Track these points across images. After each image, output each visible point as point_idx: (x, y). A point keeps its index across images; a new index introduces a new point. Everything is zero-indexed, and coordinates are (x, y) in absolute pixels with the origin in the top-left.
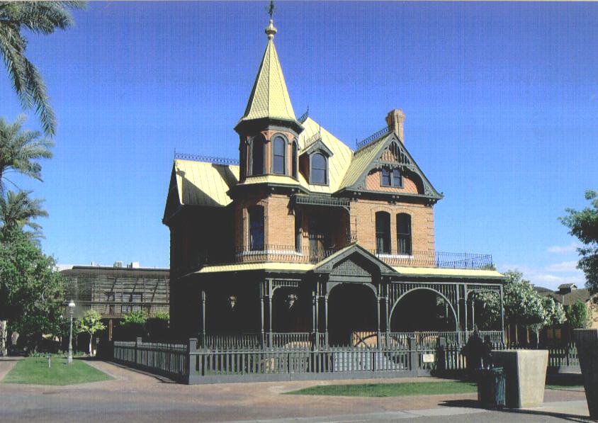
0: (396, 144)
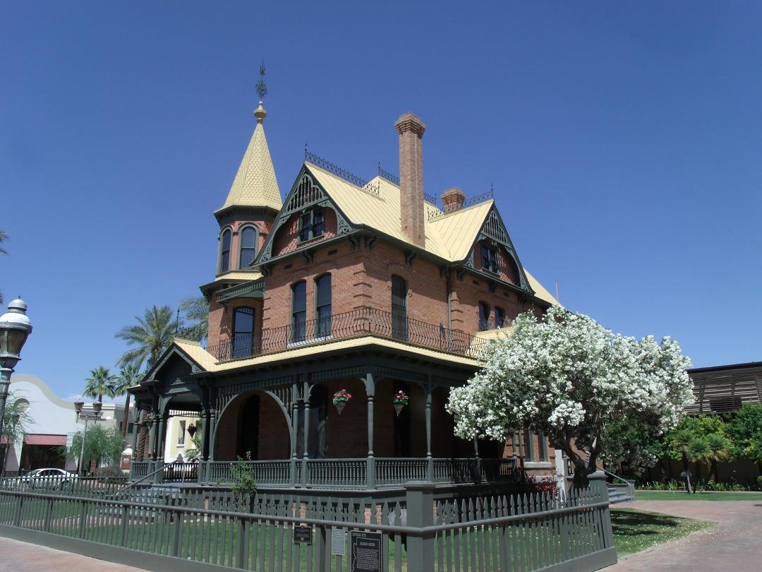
0: (307, 178)
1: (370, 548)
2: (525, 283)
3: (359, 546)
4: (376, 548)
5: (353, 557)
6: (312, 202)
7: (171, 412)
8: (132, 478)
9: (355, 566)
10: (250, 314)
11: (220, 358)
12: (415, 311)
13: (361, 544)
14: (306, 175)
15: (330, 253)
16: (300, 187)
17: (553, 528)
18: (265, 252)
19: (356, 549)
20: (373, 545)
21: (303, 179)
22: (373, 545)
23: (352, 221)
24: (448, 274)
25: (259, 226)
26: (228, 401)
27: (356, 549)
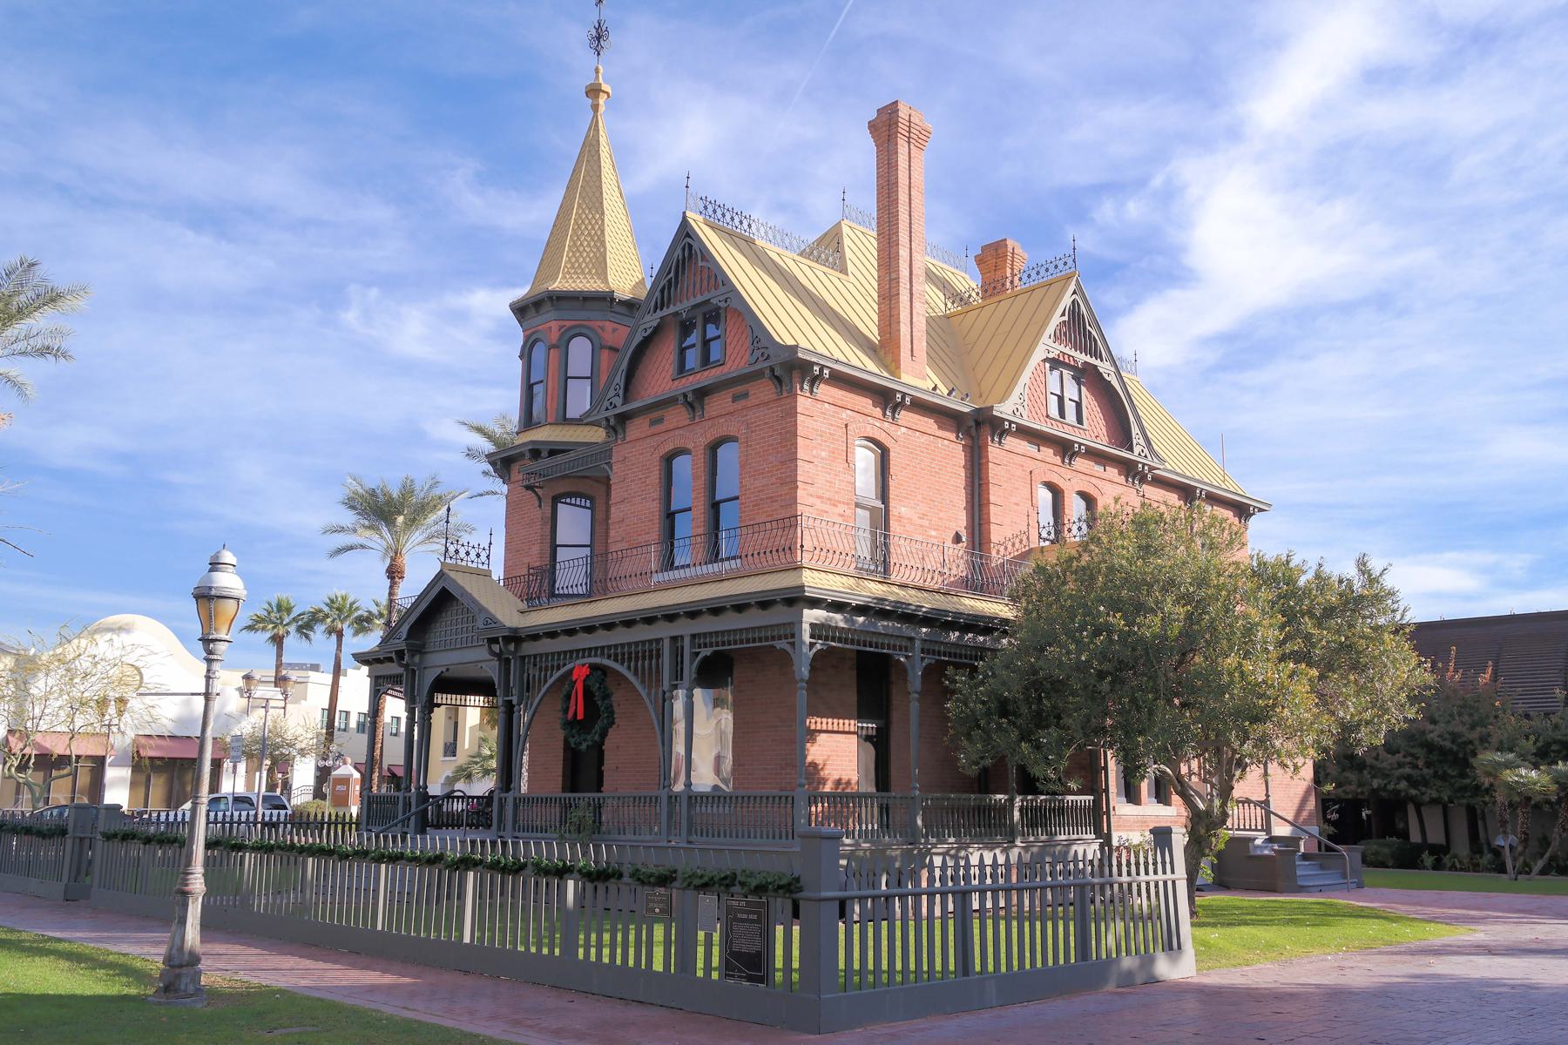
1: (752, 921)
2: (1142, 441)
3: (736, 919)
4: (758, 921)
5: (727, 936)
6: (692, 299)
7: (439, 698)
8: (368, 824)
9: (731, 948)
10: (585, 507)
11: (529, 599)
12: (903, 509)
13: (739, 916)
14: (688, 240)
15: (735, 399)
16: (678, 260)
17: (214, 866)
18: (612, 393)
19: (731, 924)
20: (755, 917)
21: (684, 249)
22: (755, 917)
23: (204, 701)
24: (973, 432)
25: (600, 331)
26: (551, 676)
27: (731, 924)
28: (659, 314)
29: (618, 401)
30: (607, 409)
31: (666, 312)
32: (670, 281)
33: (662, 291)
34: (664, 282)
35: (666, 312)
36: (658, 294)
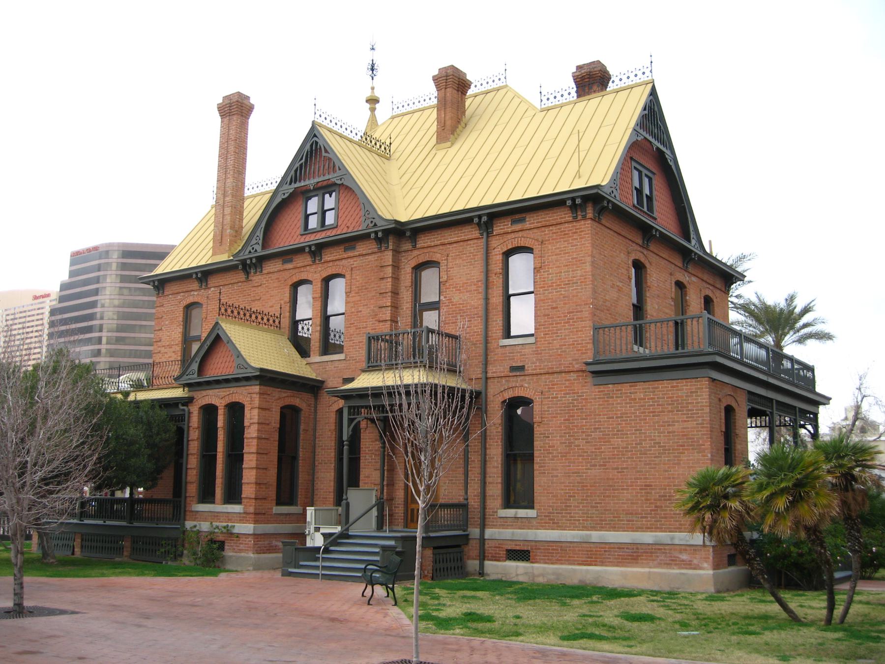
14: (315, 139)
21: (312, 146)
28: (294, 186)
29: (258, 248)
30: (250, 252)
31: (298, 185)
32: (301, 165)
33: (296, 171)
34: (297, 165)
35: (298, 185)
36: (293, 172)
